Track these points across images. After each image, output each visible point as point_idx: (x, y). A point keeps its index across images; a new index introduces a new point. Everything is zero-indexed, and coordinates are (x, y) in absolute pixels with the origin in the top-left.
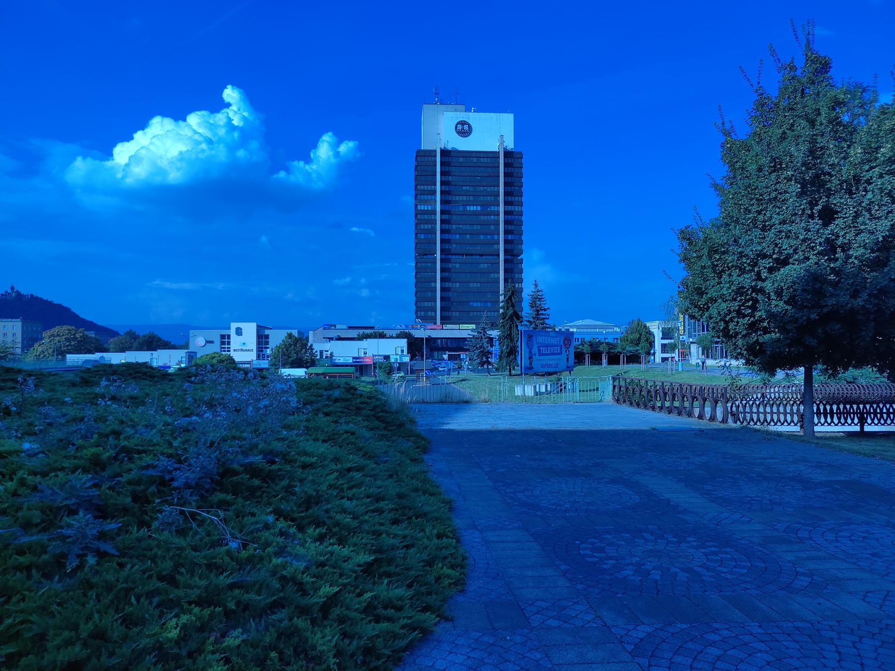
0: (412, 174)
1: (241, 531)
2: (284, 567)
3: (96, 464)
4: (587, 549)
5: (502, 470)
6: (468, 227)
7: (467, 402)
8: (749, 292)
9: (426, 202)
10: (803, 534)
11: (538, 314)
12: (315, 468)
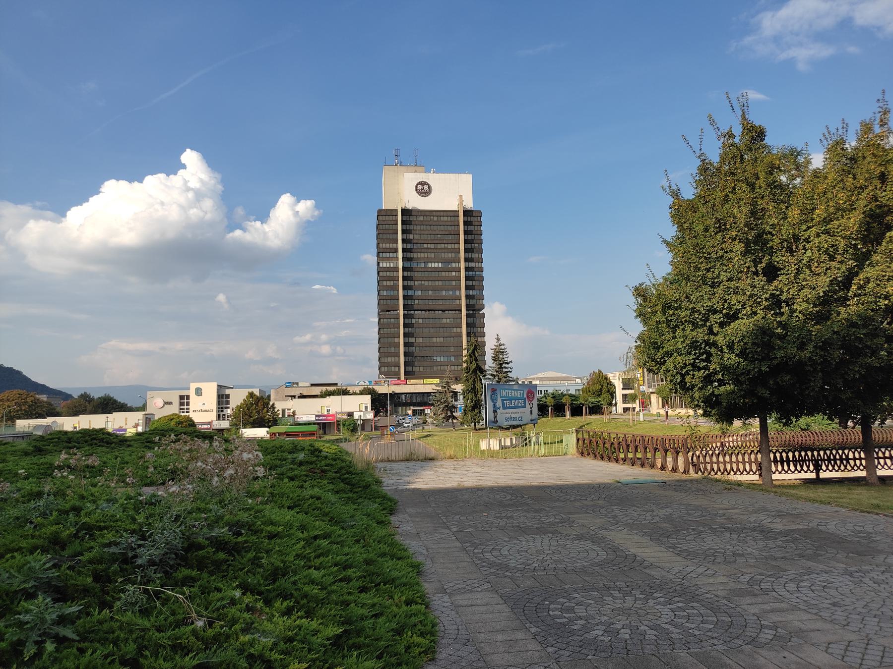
0: (374, 233)
1: (207, 609)
2: (251, 644)
3: (56, 543)
4: (556, 609)
5: (470, 530)
6: (430, 283)
7: (432, 459)
8: (703, 346)
9: (388, 260)
10: (766, 586)
11: (501, 368)
12: (281, 538)
